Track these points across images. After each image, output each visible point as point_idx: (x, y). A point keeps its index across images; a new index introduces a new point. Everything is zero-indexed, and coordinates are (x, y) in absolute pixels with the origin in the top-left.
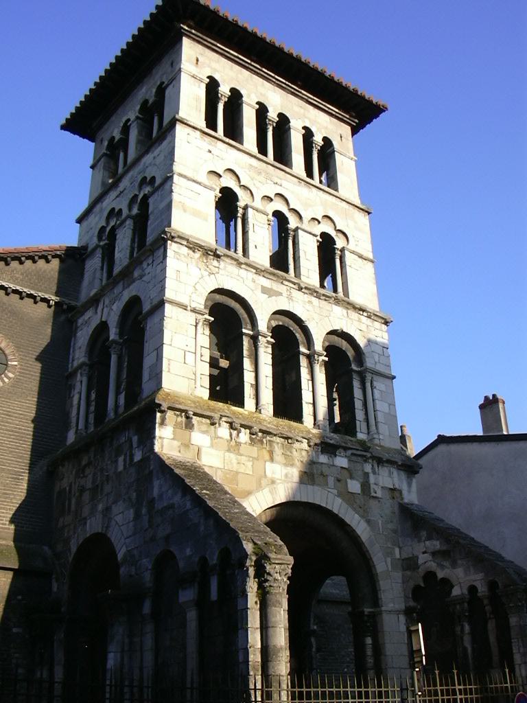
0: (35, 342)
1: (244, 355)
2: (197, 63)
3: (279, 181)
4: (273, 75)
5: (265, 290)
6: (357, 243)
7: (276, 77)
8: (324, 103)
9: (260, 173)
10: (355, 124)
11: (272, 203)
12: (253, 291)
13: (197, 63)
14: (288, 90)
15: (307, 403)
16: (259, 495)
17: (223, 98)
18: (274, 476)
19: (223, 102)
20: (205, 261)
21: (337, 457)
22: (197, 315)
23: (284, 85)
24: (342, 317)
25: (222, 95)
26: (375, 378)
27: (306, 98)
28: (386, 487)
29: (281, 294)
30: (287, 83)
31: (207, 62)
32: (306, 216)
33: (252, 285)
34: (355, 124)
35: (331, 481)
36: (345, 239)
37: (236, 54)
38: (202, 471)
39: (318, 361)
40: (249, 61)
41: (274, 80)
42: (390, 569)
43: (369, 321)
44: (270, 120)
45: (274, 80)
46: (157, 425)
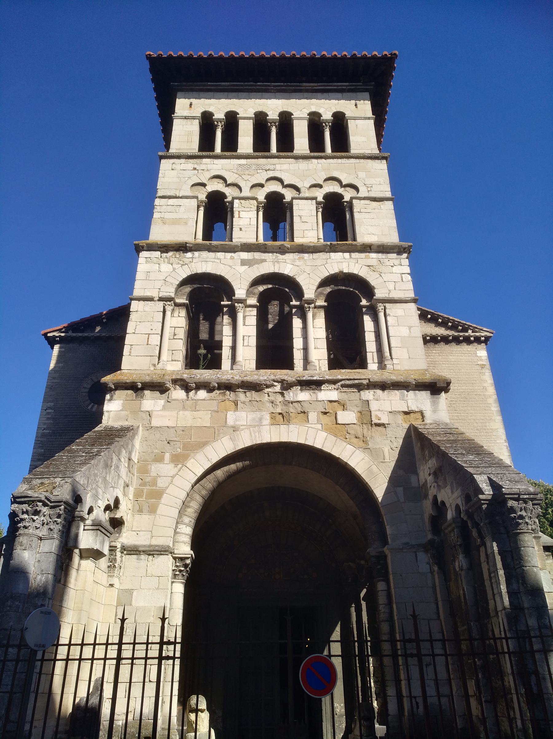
3: (272, 167)
5: (244, 263)
6: (369, 189)
12: (230, 266)
15: (298, 350)
16: (217, 445)
17: (219, 124)
18: (238, 423)
19: (220, 127)
20: (178, 256)
21: (323, 391)
24: (343, 260)
26: (387, 305)
28: (399, 412)
33: (230, 262)
35: (313, 416)
42: (402, 499)
46: (106, 402)
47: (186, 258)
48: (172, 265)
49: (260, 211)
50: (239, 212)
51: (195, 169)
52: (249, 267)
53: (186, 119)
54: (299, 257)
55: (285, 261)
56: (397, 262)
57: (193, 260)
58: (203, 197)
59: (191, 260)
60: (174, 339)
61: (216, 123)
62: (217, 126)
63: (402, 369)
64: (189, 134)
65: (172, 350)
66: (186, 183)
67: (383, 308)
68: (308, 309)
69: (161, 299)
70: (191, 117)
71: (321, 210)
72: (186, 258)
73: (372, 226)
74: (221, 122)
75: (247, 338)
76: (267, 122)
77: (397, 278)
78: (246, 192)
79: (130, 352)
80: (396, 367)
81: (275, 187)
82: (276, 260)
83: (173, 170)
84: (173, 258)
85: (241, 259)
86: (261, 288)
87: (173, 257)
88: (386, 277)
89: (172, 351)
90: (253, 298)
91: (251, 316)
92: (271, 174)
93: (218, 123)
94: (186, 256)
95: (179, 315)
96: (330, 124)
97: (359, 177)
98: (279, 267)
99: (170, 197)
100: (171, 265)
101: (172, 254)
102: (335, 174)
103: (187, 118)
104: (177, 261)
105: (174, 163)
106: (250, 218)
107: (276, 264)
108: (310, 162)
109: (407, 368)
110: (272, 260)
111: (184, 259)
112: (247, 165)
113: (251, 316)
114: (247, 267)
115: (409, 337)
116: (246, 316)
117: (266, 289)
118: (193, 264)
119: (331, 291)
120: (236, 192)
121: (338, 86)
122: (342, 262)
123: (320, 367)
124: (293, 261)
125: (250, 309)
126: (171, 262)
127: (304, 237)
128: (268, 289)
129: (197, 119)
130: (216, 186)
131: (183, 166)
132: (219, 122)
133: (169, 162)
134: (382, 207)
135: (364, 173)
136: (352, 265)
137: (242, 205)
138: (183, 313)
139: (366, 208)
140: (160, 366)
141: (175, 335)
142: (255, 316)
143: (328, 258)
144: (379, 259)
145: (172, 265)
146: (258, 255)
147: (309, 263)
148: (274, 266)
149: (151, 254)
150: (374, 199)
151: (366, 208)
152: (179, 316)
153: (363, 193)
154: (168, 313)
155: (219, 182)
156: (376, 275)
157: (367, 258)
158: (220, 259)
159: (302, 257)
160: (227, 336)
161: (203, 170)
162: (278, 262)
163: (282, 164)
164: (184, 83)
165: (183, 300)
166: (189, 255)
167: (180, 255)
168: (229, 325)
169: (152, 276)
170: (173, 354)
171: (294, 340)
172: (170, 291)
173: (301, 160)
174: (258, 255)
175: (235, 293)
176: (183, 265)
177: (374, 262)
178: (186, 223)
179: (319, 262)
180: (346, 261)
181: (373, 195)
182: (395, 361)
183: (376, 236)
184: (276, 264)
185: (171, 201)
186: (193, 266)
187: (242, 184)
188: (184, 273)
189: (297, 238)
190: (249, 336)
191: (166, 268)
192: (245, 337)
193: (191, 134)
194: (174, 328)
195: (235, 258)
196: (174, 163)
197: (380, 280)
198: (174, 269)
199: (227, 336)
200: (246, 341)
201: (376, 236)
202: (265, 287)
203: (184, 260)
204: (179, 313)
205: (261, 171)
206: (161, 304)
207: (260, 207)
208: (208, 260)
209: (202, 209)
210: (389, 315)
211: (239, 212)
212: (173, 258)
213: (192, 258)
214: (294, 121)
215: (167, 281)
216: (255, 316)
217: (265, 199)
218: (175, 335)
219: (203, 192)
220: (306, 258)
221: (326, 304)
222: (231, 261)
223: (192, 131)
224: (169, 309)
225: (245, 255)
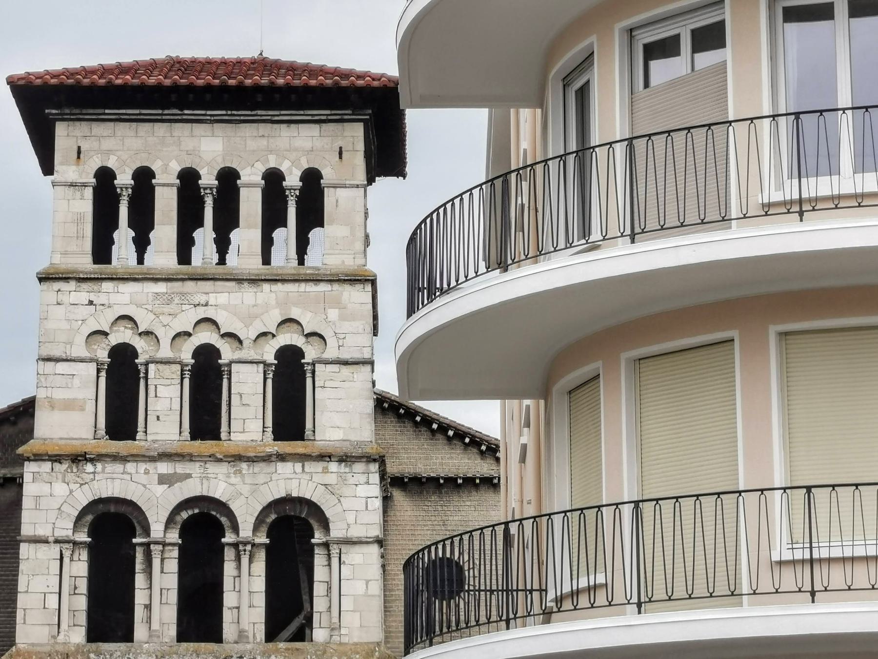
0: (4, 537)
1: (137, 571)
2: (79, 157)
4: (203, 112)
5: (163, 480)
7: (209, 112)
8: (302, 112)
9: (169, 302)
10: (368, 117)
11: (191, 338)
12: (144, 486)
13: (79, 157)
14: (236, 120)
19: (126, 198)
20: (75, 470)
22: (62, 545)
23: (227, 118)
24: (293, 476)
25: (121, 188)
26: (344, 548)
27: (269, 118)
29: (189, 476)
30: (229, 112)
31: (95, 145)
32: (248, 334)
33: (143, 479)
34: (368, 117)
36: (323, 342)
37: (137, 111)
38: (411, 650)
39: (245, 550)
40: (160, 112)
41: (209, 118)
43: (343, 468)
44: (205, 189)
45: (209, 118)
47: (86, 473)
48: (68, 485)
49: (185, 377)
50: (156, 386)
51: (91, 303)
52: (169, 487)
53: (73, 186)
54: (235, 469)
55: (216, 476)
56: (363, 478)
57: (95, 476)
58: (103, 355)
59: (92, 476)
60: (75, 594)
61: (118, 190)
62: (120, 195)
63: (351, 642)
64: (79, 221)
65: (74, 611)
66: (79, 331)
67: (338, 552)
68: (243, 553)
69: (57, 541)
70: (80, 183)
71: (271, 376)
72: (86, 473)
73: (337, 412)
74: (127, 188)
75: (166, 593)
76: (200, 188)
77: (359, 504)
78: (165, 351)
79: (24, 619)
80: (345, 640)
81: (206, 336)
82: (204, 475)
83: (59, 304)
84: (68, 472)
85: (159, 474)
86: (185, 515)
87: (69, 471)
88: (347, 503)
89: (73, 612)
90: (174, 530)
91: (171, 558)
92: (202, 313)
93: (122, 190)
94: (85, 470)
95: (79, 559)
96: (297, 193)
97: (329, 319)
98: (209, 487)
99: (57, 360)
100: (66, 485)
101: (67, 466)
102: (295, 314)
103: (74, 184)
104: (74, 477)
105: (59, 290)
106: (171, 399)
107: (205, 481)
108: (259, 289)
109: (356, 640)
110: (199, 475)
111: (84, 476)
112: (167, 295)
113: (171, 558)
114: (166, 486)
115: (364, 595)
116: (165, 558)
117: (191, 515)
118: (95, 482)
119: (276, 518)
120: (152, 346)
121: (312, 115)
122: (291, 479)
123: (254, 634)
124: (227, 477)
125: (170, 548)
126: (66, 481)
127: (244, 432)
128: (194, 515)
129: (90, 186)
130: (122, 335)
131: (75, 297)
132: (124, 189)
133: (53, 289)
134: (355, 376)
135: (337, 310)
136: (304, 482)
137: (161, 374)
138: (84, 555)
139: (332, 380)
140: (61, 639)
141: (76, 588)
142: (176, 558)
143: (274, 471)
144: (341, 474)
145: (68, 485)
146: (181, 468)
147: (248, 480)
148: (202, 484)
149: (40, 467)
150: (346, 363)
151: (332, 380)
152: (79, 560)
153: (331, 353)
154: (66, 560)
155: (127, 326)
156: (333, 500)
157: (326, 473)
158: (130, 474)
159: (238, 470)
160: (141, 589)
161: (103, 305)
162: (208, 478)
163: (218, 293)
164: (67, 111)
165: (83, 537)
166: (89, 467)
167: (77, 467)
168: (143, 573)
169: (44, 504)
170: (74, 615)
171: (225, 595)
172: (65, 528)
173: (246, 284)
174: (181, 466)
175: (150, 528)
176: (82, 485)
177: (332, 479)
178: (82, 409)
179: (261, 479)
180: (297, 476)
181: (345, 355)
182: (343, 631)
183: (341, 431)
184: (205, 481)
185: (61, 367)
186: (96, 487)
187: (160, 332)
188: (83, 498)
189: (234, 432)
190: (168, 589)
191: (60, 489)
192: (163, 590)
193: (82, 221)
194: (74, 578)
195: (150, 472)
196: (59, 290)
197: (339, 507)
198: (71, 492)
199: (141, 589)
200: (164, 597)
201: (341, 431)
202: (190, 512)
203: (84, 477)
204: (80, 554)
205: (188, 307)
206: (56, 548)
207: (186, 370)
208: (115, 476)
209: (103, 374)
210: (344, 562)
211: (156, 386)
212: (68, 472)
213: (94, 473)
214: (241, 189)
215: (64, 512)
216: (176, 558)
217: (193, 358)
218: (76, 588)
219: (105, 346)
220: (244, 472)
221: (267, 541)
222: (146, 476)
223: (84, 213)
224: (67, 554)
225: (164, 468)
